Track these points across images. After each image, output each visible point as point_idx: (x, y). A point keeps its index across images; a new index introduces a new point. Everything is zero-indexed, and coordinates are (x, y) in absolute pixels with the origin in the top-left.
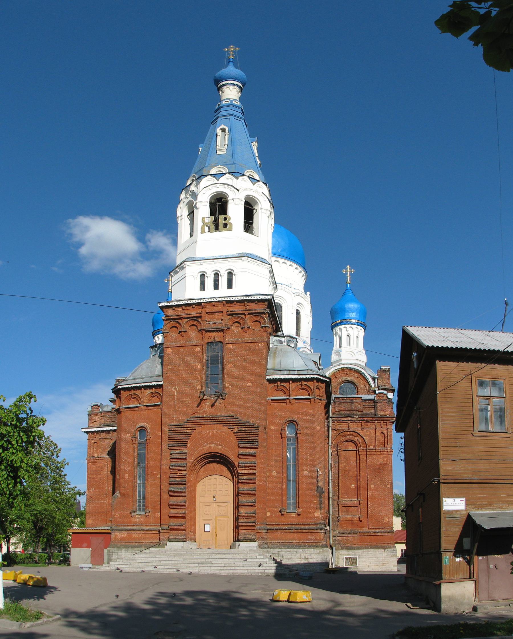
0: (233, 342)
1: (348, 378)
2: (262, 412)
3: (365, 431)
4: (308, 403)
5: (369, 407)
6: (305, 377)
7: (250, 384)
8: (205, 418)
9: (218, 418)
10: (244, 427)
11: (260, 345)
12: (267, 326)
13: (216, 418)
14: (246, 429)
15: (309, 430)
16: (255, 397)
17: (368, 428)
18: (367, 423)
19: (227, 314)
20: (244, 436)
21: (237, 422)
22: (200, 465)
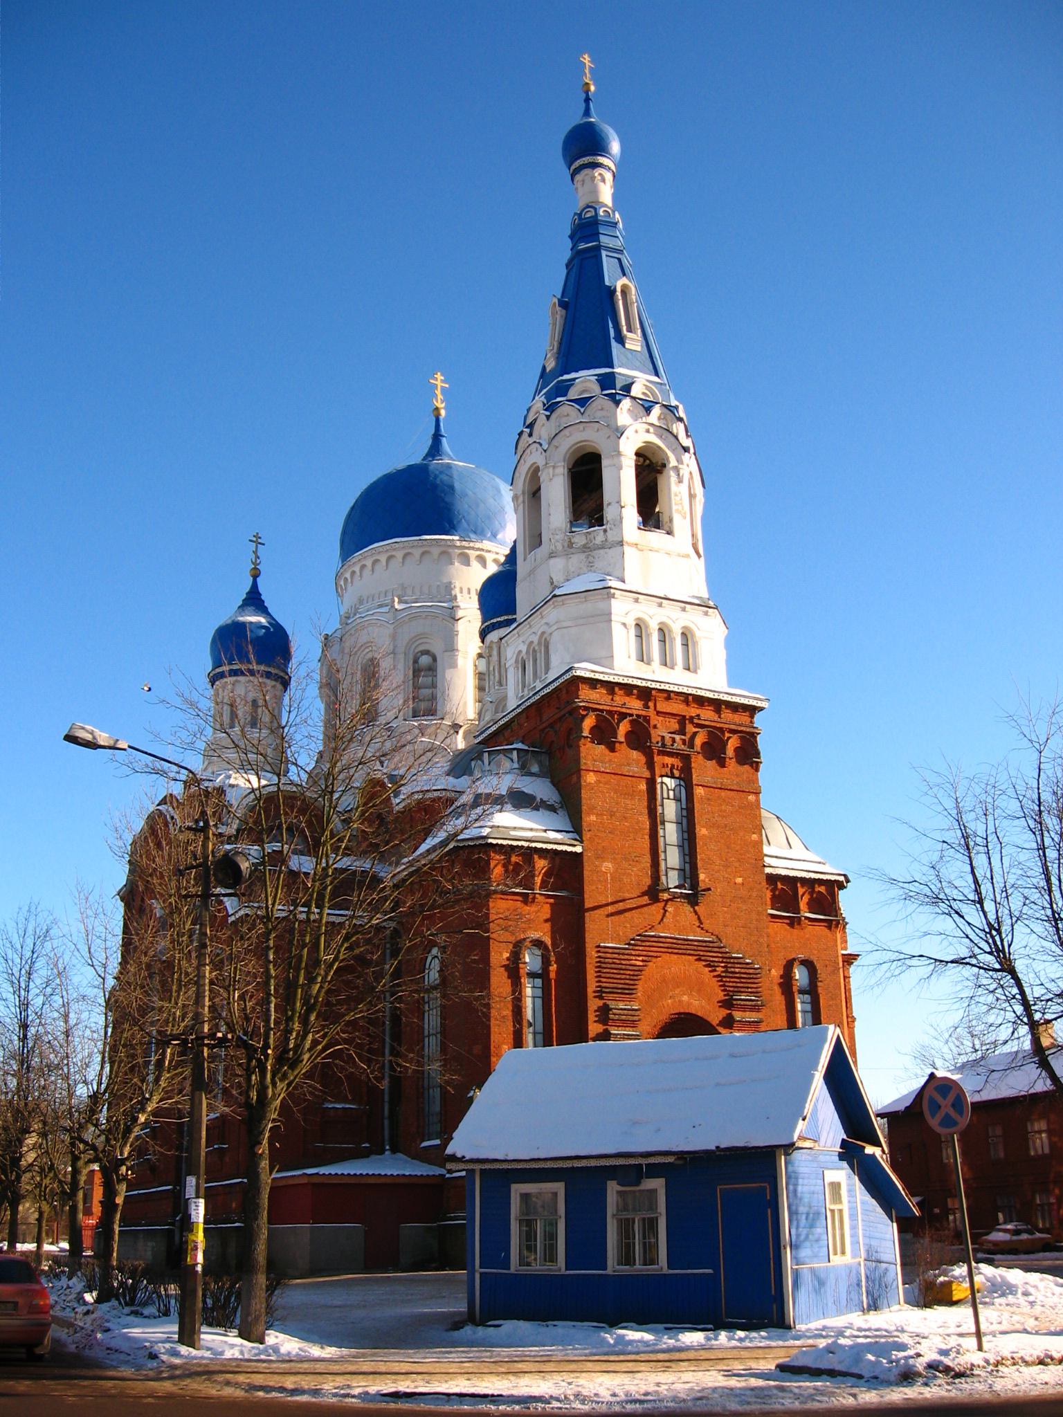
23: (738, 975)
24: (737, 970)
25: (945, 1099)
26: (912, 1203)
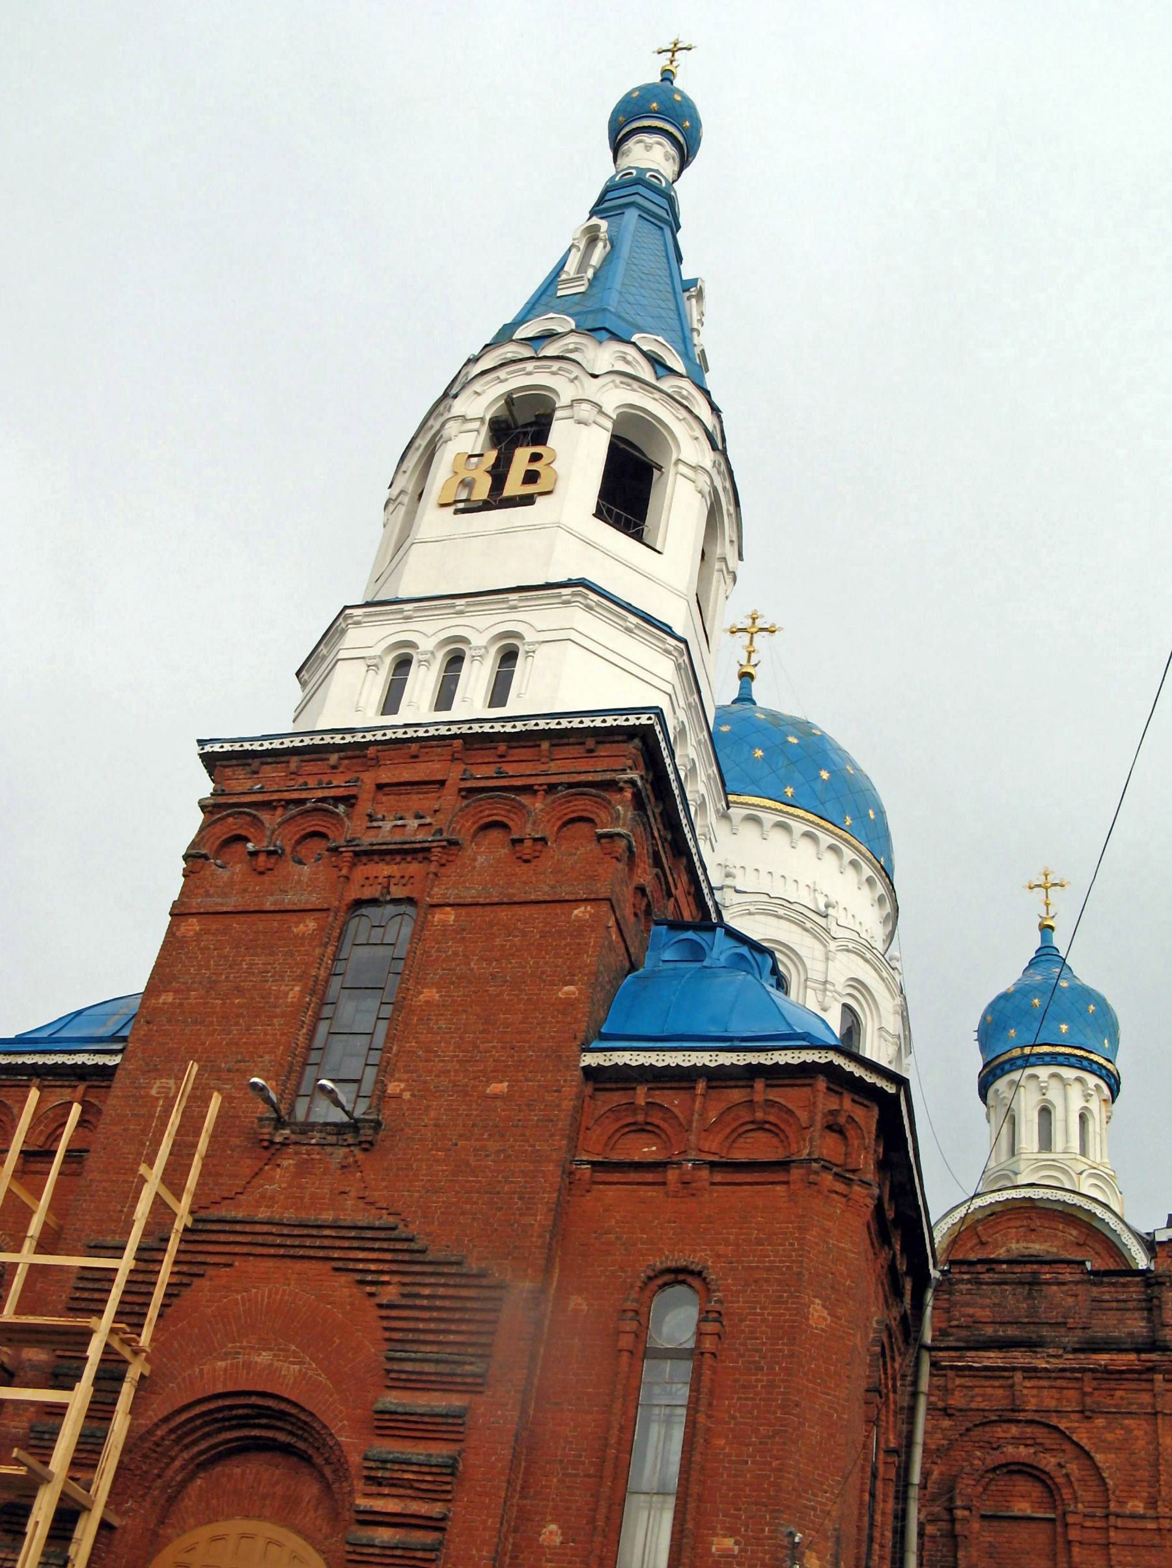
1: (1037, 1246)
2: (535, 1215)
3: (1100, 1422)
4: (778, 1188)
5: (1122, 1305)
6: (769, 1063)
8: (258, 1228)
9: (314, 1232)
10: (432, 1280)
11: (576, 912)
12: (619, 835)
13: (305, 1232)
15: (764, 1320)
16: (512, 1147)
17: (1116, 1406)
18: (1113, 1384)
20: (421, 1326)
21: (400, 1257)
22: (186, 1455)
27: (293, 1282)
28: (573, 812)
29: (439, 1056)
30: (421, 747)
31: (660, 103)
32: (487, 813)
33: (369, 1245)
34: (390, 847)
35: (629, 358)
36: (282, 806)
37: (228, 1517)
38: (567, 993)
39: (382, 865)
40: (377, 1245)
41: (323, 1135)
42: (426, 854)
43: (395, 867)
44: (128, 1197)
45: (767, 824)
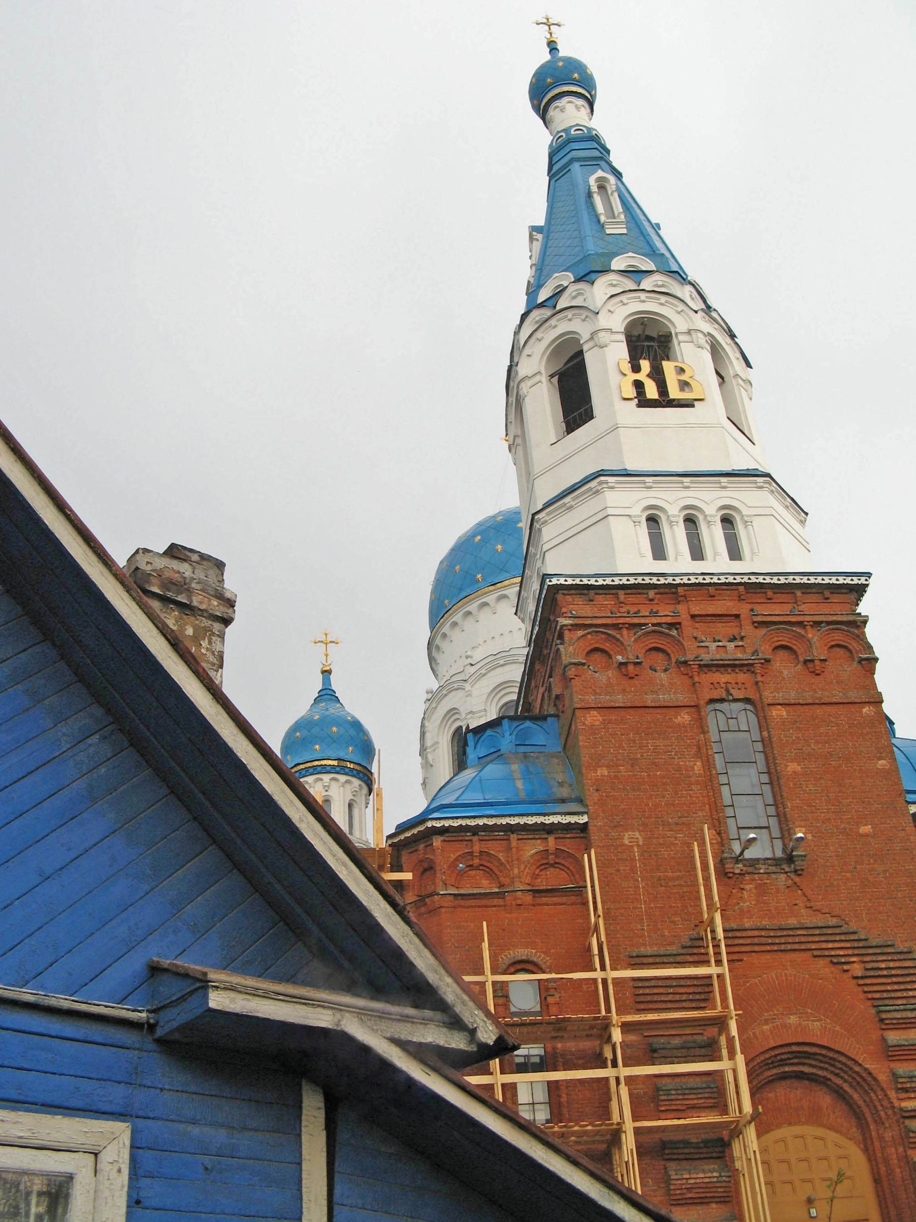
0: (787, 702)
7: (866, 829)
9: (791, 933)
14: (892, 964)
19: (754, 622)
21: (856, 944)
23: (885, 973)
24: (883, 965)
25: (70, 1177)
26: (586, 856)
27: (789, 967)
28: (832, 641)
29: (819, 809)
30: (717, 590)
31: (552, 76)
32: (776, 639)
33: (831, 938)
34: (726, 662)
35: (615, 282)
36: (627, 628)
37: (779, 1126)
38: (881, 765)
39: (717, 674)
40: (837, 938)
41: (766, 867)
42: (750, 668)
43: (728, 676)
44: (642, 919)
45: (492, 603)
